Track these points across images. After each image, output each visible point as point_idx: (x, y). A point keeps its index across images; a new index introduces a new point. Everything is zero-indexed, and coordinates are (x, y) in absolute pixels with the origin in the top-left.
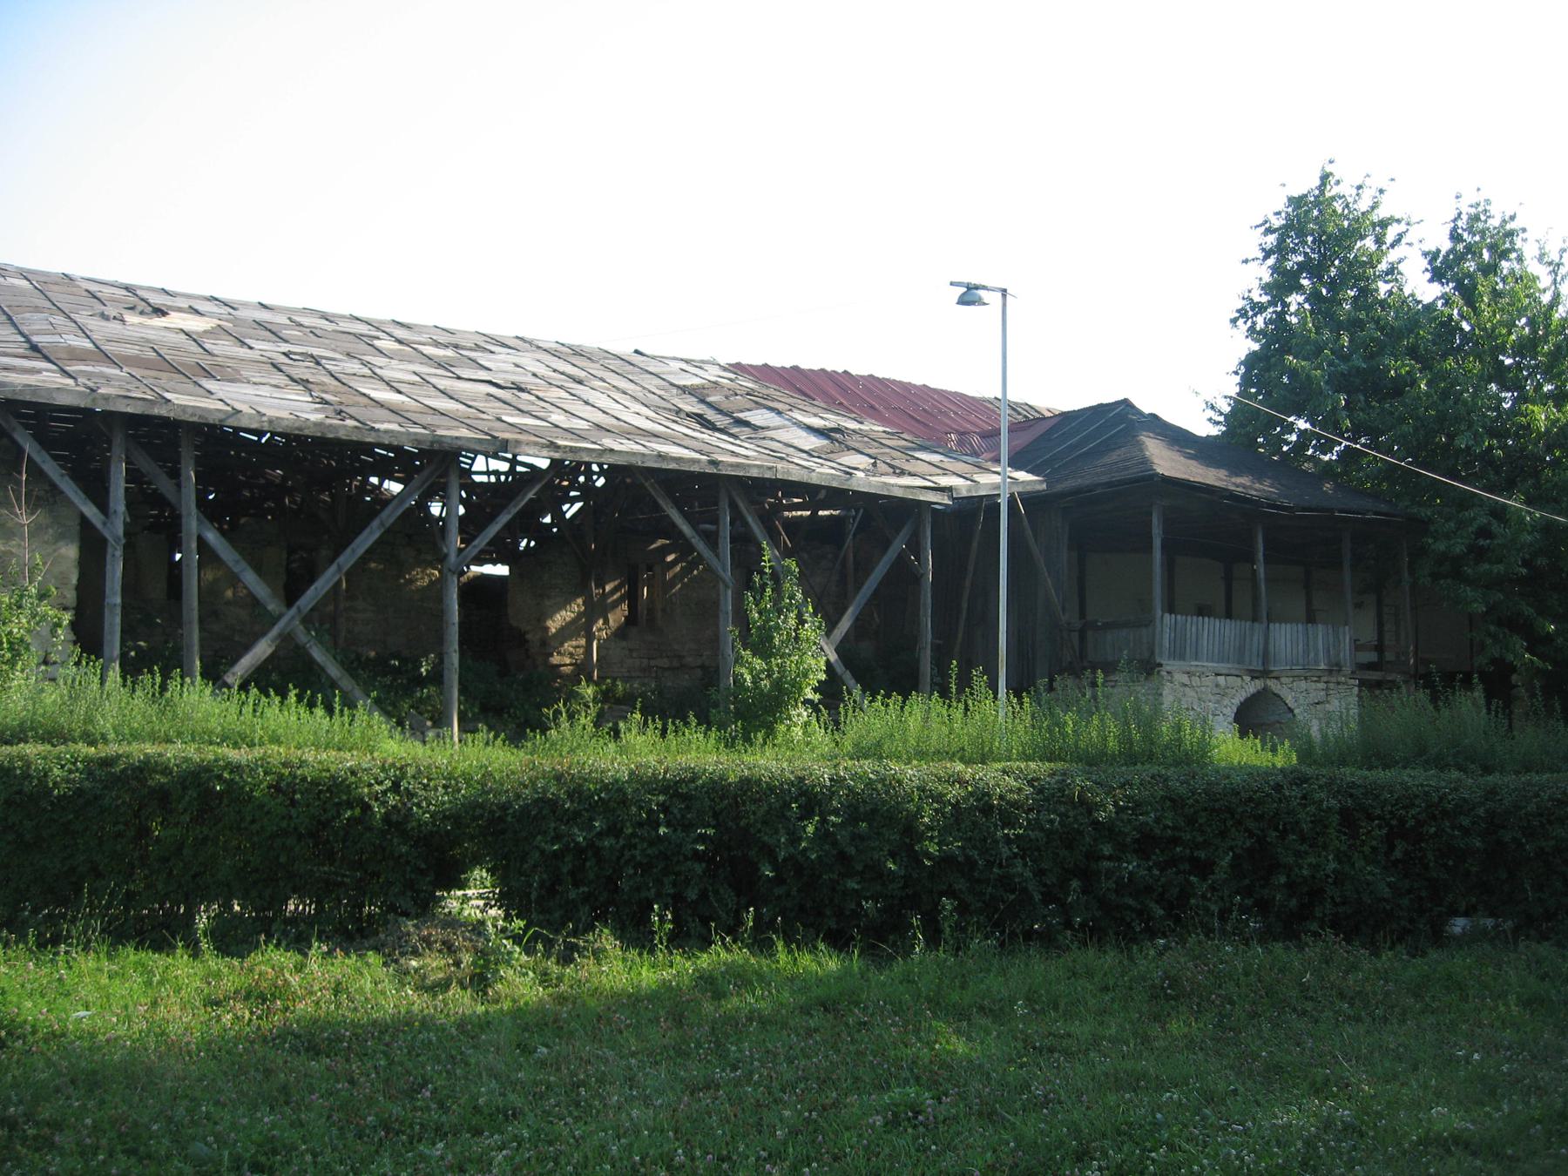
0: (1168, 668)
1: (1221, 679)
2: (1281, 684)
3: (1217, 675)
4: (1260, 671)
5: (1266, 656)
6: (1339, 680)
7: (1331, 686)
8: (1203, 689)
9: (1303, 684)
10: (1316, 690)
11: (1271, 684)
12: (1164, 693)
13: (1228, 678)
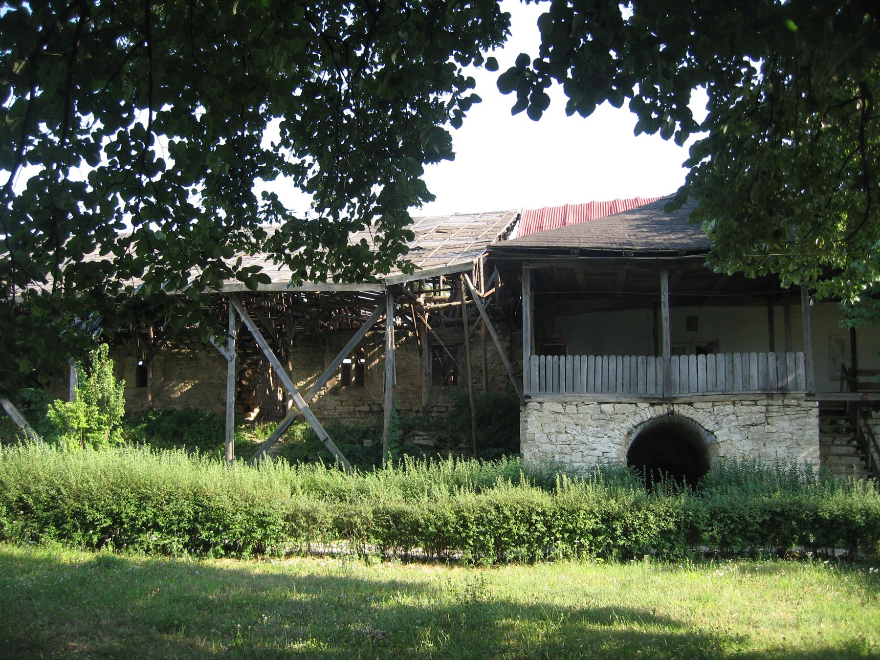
0: (540, 399)
1: (607, 408)
2: (696, 408)
3: (600, 403)
4: (659, 398)
5: (668, 381)
6: (786, 402)
7: (775, 409)
8: (581, 416)
9: (729, 408)
10: (753, 412)
11: (683, 410)
12: (529, 420)
13: (616, 406)
